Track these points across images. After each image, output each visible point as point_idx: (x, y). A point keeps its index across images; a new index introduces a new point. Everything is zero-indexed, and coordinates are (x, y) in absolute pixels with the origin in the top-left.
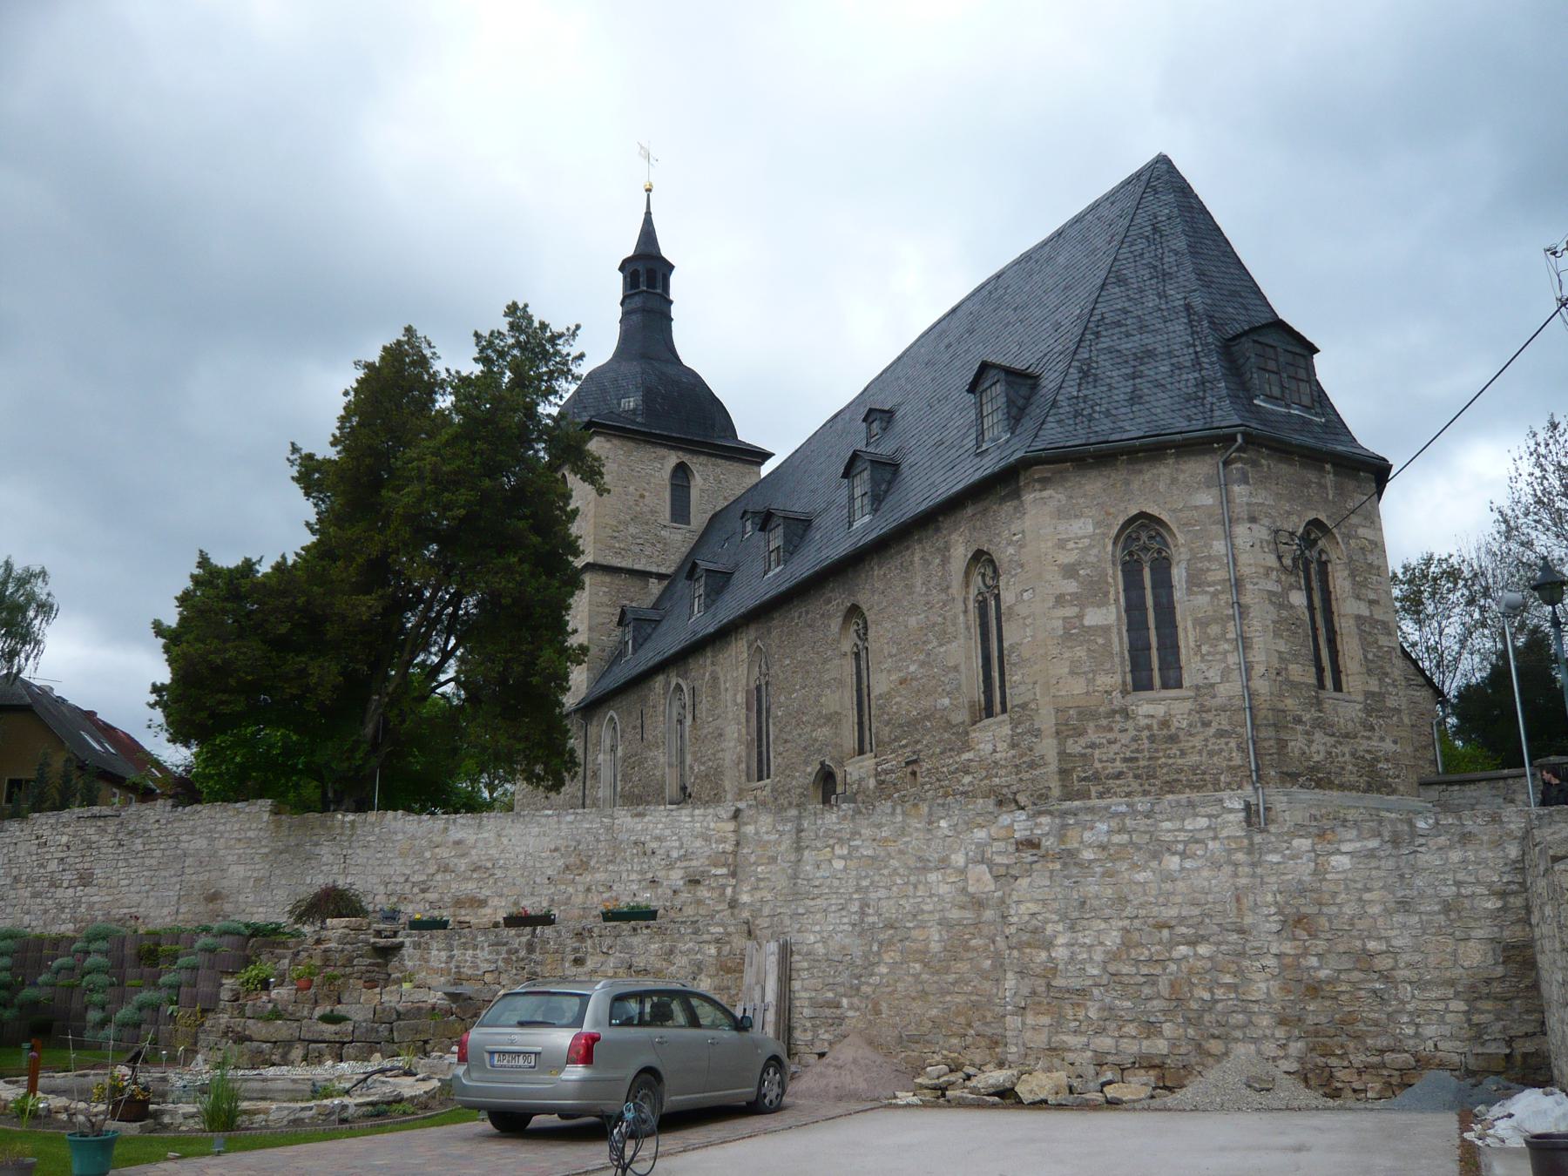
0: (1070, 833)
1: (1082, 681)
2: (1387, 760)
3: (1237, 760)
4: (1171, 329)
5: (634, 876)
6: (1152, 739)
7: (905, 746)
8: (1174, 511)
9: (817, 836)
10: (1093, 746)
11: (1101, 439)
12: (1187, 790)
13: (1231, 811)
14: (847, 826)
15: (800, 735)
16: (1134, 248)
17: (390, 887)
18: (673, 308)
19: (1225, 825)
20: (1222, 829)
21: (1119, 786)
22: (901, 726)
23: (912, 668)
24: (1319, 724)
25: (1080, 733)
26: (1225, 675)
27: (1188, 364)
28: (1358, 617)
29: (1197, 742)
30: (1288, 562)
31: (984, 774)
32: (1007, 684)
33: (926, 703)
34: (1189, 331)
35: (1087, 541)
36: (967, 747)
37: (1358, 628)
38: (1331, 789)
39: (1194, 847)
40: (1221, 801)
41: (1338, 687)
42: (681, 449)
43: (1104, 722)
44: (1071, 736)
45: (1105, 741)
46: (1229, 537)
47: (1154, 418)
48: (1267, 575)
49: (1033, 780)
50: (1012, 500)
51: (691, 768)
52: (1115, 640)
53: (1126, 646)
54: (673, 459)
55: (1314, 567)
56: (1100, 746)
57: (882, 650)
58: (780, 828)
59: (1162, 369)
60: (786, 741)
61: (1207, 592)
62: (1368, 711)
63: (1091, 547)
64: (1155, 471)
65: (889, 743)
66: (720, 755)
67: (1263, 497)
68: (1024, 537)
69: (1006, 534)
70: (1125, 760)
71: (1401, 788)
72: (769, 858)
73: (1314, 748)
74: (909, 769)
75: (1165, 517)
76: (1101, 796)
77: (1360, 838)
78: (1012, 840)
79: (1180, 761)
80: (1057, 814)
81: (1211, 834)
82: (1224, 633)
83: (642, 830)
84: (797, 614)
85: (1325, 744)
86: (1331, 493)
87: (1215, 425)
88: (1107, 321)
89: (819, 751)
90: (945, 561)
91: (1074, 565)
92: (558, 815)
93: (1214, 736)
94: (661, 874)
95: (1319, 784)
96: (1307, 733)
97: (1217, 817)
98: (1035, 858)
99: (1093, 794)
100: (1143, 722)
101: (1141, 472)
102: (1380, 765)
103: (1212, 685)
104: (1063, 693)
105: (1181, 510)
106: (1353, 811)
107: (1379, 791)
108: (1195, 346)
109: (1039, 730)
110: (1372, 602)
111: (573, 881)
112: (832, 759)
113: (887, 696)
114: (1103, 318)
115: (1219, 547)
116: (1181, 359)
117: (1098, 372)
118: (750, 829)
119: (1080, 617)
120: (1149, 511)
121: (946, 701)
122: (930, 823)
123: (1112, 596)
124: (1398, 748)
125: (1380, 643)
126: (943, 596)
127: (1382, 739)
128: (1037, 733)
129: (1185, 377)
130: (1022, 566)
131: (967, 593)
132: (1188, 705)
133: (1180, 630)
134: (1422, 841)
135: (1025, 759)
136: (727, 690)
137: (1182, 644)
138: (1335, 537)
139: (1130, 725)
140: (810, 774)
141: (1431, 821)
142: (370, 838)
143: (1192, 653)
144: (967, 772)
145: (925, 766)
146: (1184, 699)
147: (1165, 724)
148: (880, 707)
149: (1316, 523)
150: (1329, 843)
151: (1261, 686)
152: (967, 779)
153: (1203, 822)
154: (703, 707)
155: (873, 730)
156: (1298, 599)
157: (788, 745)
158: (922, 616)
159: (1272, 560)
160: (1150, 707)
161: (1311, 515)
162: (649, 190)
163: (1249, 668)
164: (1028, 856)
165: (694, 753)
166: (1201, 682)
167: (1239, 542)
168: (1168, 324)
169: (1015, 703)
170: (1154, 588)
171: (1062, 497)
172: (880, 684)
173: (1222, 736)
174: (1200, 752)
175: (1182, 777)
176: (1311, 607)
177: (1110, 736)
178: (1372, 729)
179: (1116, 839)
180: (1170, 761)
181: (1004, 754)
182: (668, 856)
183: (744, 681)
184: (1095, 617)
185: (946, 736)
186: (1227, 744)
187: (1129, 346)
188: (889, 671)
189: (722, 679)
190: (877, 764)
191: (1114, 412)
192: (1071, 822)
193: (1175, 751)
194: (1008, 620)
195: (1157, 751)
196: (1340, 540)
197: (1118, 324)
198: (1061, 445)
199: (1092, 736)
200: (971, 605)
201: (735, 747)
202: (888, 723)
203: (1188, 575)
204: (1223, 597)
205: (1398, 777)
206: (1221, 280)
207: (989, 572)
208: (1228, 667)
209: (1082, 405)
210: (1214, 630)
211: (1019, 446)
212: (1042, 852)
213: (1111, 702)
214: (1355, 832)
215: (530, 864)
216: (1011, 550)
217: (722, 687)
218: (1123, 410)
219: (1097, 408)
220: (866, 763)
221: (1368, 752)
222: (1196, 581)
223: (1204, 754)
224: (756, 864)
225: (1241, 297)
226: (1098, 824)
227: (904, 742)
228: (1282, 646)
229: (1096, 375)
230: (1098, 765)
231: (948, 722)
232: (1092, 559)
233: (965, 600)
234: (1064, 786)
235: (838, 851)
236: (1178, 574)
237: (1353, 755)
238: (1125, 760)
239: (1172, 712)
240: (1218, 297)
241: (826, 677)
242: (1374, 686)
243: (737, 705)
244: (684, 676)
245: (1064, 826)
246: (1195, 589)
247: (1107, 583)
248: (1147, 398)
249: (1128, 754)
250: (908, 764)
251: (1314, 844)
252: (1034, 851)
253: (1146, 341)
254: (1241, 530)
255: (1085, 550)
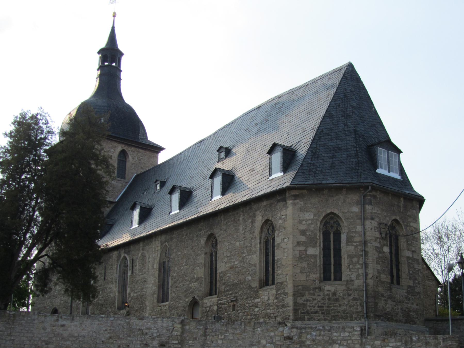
0: (303, 335)
1: (305, 275)
2: (414, 312)
3: (360, 309)
4: (348, 139)
5: (138, 342)
6: (329, 299)
7: (231, 294)
8: (344, 213)
9: (212, 331)
10: (307, 300)
11: (319, 182)
12: (341, 319)
13: (356, 331)
14: (224, 328)
15: (184, 285)
16: (336, 102)
17: (32, 341)
18: (122, 73)
19: (354, 335)
20: (353, 337)
21: (316, 316)
22: (230, 286)
23: (236, 263)
24: (390, 297)
25: (303, 295)
26: (358, 277)
27: (354, 155)
28: (408, 257)
29: (346, 302)
30: (384, 235)
31: (264, 308)
32: (276, 274)
33: (241, 277)
34: (355, 141)
35: (310, 222)
36: (257, 296)
37: (407, 261)
38: (392, 322)
39: (343, 342)
40: (353, 327)
41: (398, 283)
42: (123, 143)
43: (312, 292)
44: (299, 296)
45: (312, 299)
46: (364, 225)
47: (339, 176)
48: (376, 240)
49: (283, 312)
50: (282, 202)
51: (130, 294)
52: (318, 261)
53: (322, 263)
54: (119, 148)
55: (394, 237)
56: (310, 301)
57: (223, 254)
58: (199, 327)
59: (343, 155)
60: (177, 287)
61: (353, 245)
62: (408, 293)
63: (312, 224)
64: (338, 197)
65: (225, 292)
66: (144, 290)
67: (377, 210)
68: (286, 217)
69: (279, 215)
70: (319, 307)
71: (418, 322)
72: (194, 338)
73: (388, 306)
74: (232, 304)
75: (340, 215)
76: (309, 320)
77: (395, 342)
78: (283, 337)
79: (339, 308)
80: (299, 328)
81: (349, 338)
82: (359, 261)
83: (142, 325)
84: (185, 234)
85: (392, 305)
86: (402, 209)
87: (362, 181)
88: (324, 132)
89: (192, 292)
90: (253, 222)
91: (305, 230)
92: (107, 317)
93: (352, 300)
94: (149, 342)
95: (388, 320)
96: (385, 300)
97: (351, 332)
98: (290, 343)
99: (306, 319)
100: (326, 293)
101: (333, 196)
102: (411, 314)
103: (353, 281)
104: (297, 280)
105: (346, 213)
106: (400, 330)
107: (410, 323)
108: (357, 148)
109: (287, 293)
110: (413, 252)
111: (113, 343)
112: (198, 296)
113: (225, 273)
114: (322, 131)
115: (359, 228)
116: (351, 152)
117: (319, 154)
118: (187, 327)
119: (306, 251)
120: (335, 212)
121: (250, 278)
122: (254, 329)
123: (318, 244)
124: (418, 307)
125: (415, 267)
126: (251, 236)
127: (412, 304)
128: (286, 294)
129: (352, 160)
130: (285, 228)
131: (261, 235)
132: (343, 287)
133: (342, 258)
134: (414, 344)
135: (281, 304)
136: (149, 262)
137: (343, 264)
138: (402, 226)
139: (321, 293)
140: (187, 302)
141: (417, 338)
142: (23, 322)
143: (346, 268)
144: (257, 307)
145: (240, 303)
146: (342, 285)
147: (334, 294)
148: (221, 277)
149: (396, 220)
150: (386, 343)
151: (370, 282)
152: (257, 309)
153: (347, 334)
154: (137, 268)
155: (218, 286)
156: (386, 249)
157: (178, 289)
158: (242, 242)
159: (378, 235)
160: (329, 287)
161: (394, 217)
162: (114, 16)
163: (366, 275)
164: (288, 342)
165: (131, 288)
166: (349, 279)
167: (366, 227)
168: (347, 137)
169: (278, 282)
170: (334, 241)
171: (302, 203)
172: (221, 267)
173: (355, 300)
174: (346, 306)
175: (339, 314)
176: (391, 252)
177: (314, 297)
178: (409, 300)
179: (318, 338)
180: (335, 308)
181: (272, 301)
182: (153, 335)
183: (158, 259)
184: (312, 251)
185: (249, 292)
186: (356, 303)
187: (332, 144)
188: (226, 263)
189: (147, 257)
190: (218, 300)
191: (324, 171)
192: (304, 331)
193: (337, 305)
194: (278, 249)
195: (331, 304)
196: (404, 227)
197: (328, 134)
198: (303, 183)
199: (307, 297)
200: (262, 241)
201: (152, 287)
202: (224, 284)
203: (347, 238)
204: (359, 247)
205: (417, 318)
206: (368, 120)
207: (271, 228)
208: (359, 274)
209: (312, 167)
210: (355, 260)
211: (287, 180)
212: (293, 341)
213: (315, 284)
214: (394, 340)
215: (95, 335)
216: (280, 221)
217: (147, 260)
218: (327, 171)
219: (318, 169)
220: (213, 299)
221: (407, 308)
222: (350, 241)
223: (348, 306)
224: (189, 340)
225: (376, 127)
226: (312, 333)
227: (231, 292)
228: (379, 267)
229: (318, 155)
230: (308, 308)
231: (250, 286)
232: (312, 229)
233: (260, 238)
234: (295, 315)
235: (220, 337)
236: (344, 237)
237: (401, 309)
238: (319, 307)
239: (337, 290)
240: (367, 127)
241: (197, 262)
242: (411, 283)
243: (154, 269)
244: (128, 253)
245: (301, 333)
246: (349, 244)
247: (317, 238)
248: (337, 167)
249: (320, 305)
250: (232, 301)
251: (381, 343)
252: (290, 341)
253: (339, 143)
254: (368, 222)
255: (309, 225)
